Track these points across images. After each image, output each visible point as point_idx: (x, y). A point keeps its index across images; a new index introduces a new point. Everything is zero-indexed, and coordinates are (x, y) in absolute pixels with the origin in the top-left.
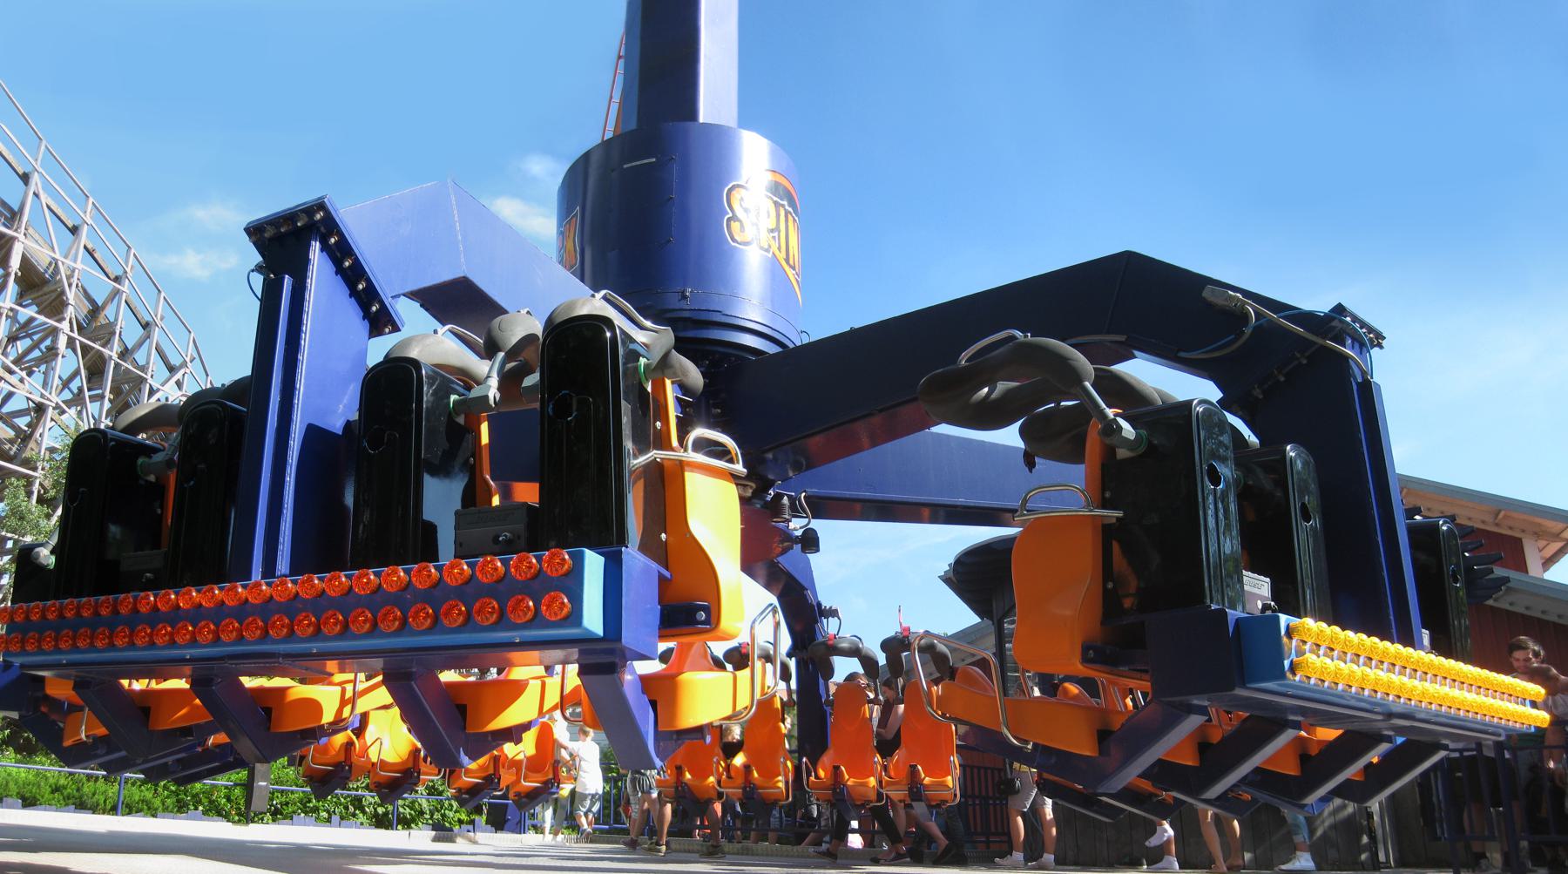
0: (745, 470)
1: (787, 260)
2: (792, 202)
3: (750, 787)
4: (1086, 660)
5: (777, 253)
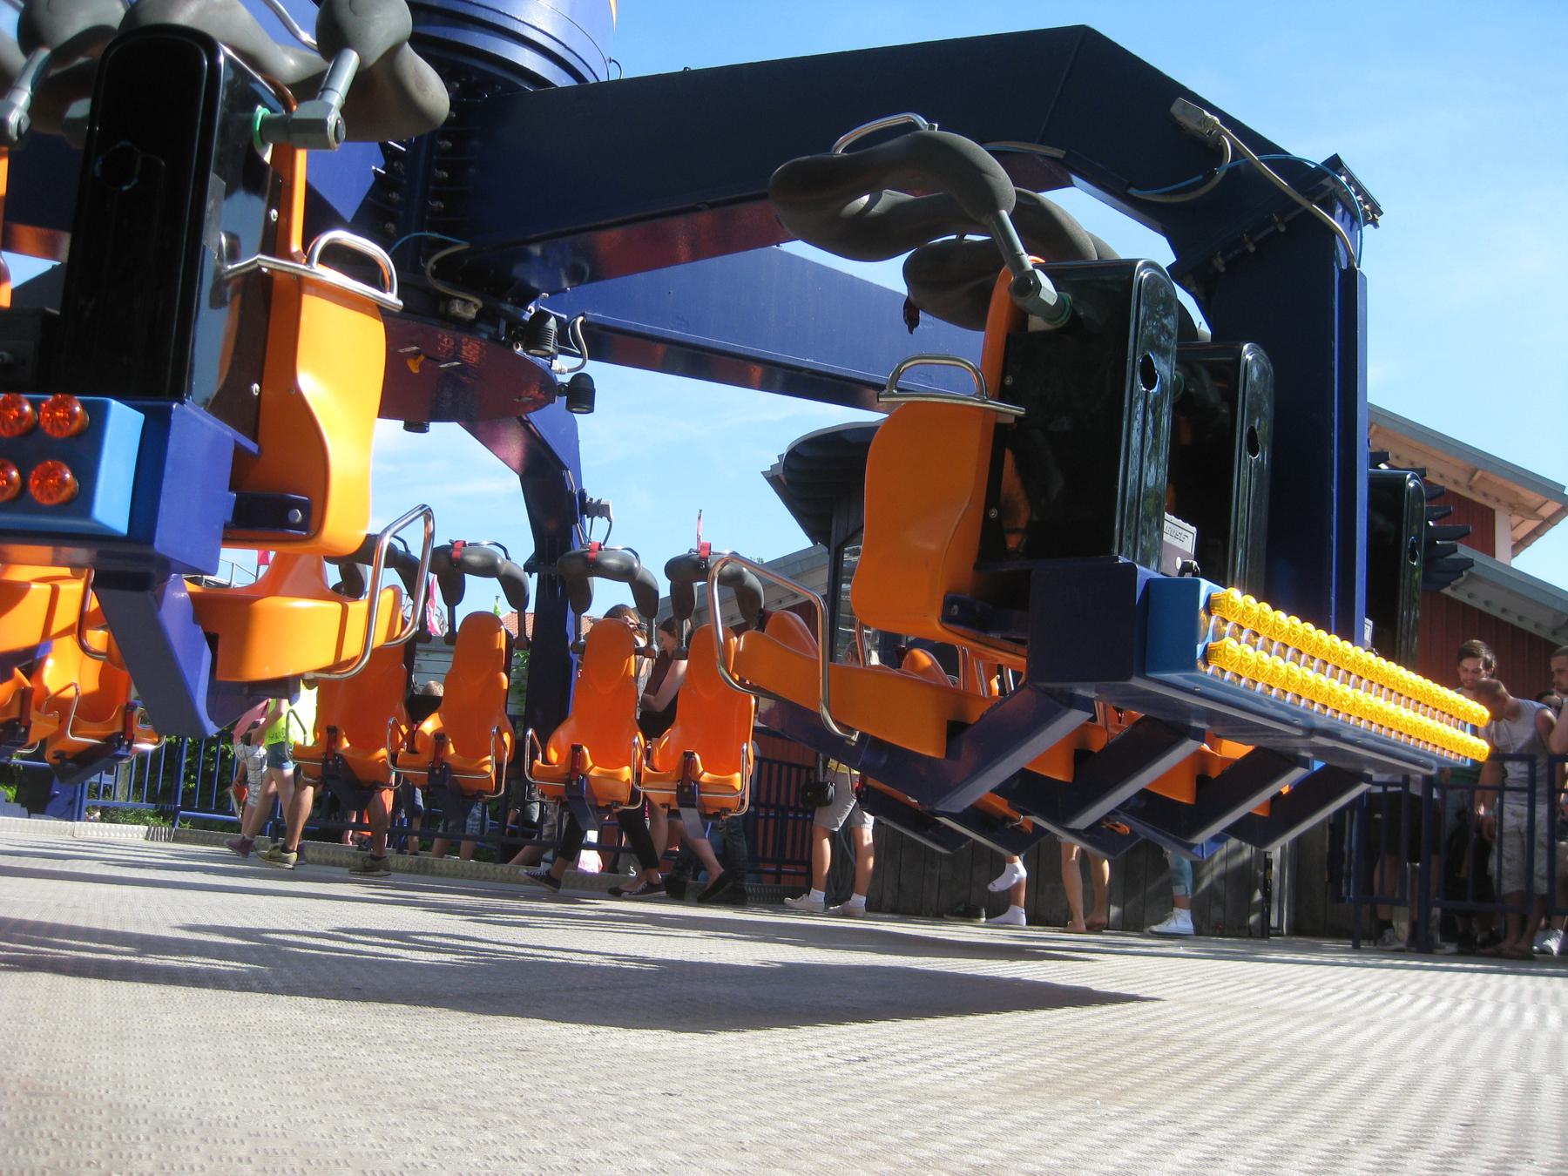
0: (400, 303)
4: (947, 619)
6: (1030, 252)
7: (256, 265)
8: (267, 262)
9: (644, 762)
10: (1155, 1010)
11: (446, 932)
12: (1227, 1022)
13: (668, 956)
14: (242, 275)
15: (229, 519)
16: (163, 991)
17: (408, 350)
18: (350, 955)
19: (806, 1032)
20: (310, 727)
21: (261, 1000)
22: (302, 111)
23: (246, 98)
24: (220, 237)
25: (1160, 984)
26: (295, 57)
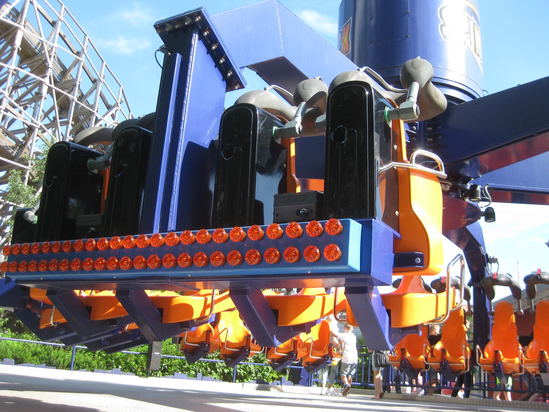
0: (446, 175)
1: (475, 50)
3: (444, 362)
5: (469, 46)
7: (392, 166)
9: (523, 356)
22: (404, 106)
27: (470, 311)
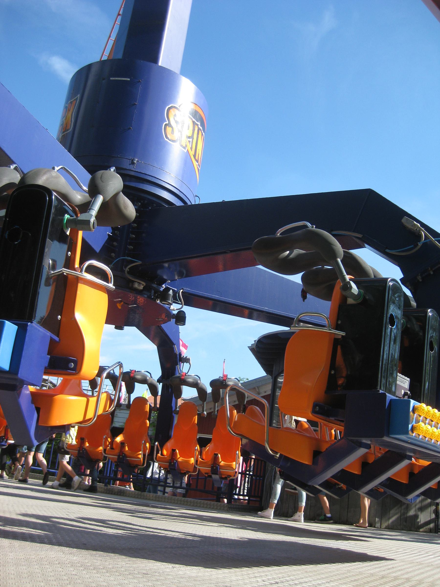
0: (114, 287)
1: (195, 156)
2: (203, 124)
3: (122, 456)
4: (314, 412)
5: (190, 150)
6: (348, 274)
7: (62, 272)
8: (66, 271)
9: (199, 456)
10: (392, 564)
11: (120, 520)
12: (420, 571)
13: (205, 534)
14: (57, 275)
15: (47, 365)
16: (11, 542)
17: (118, 300)
18: (83, 529)
19: (255, 570)
20: (74, 438)
21: (48, 547)
22: (82, 217)
23: (62, 211)
24: (49, 261)
25: (394, 553)
26: (81, 195)
27: (156, 407)
